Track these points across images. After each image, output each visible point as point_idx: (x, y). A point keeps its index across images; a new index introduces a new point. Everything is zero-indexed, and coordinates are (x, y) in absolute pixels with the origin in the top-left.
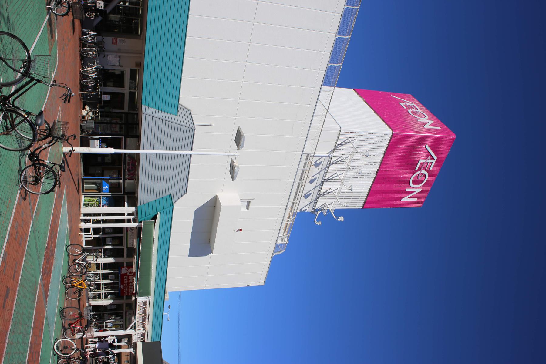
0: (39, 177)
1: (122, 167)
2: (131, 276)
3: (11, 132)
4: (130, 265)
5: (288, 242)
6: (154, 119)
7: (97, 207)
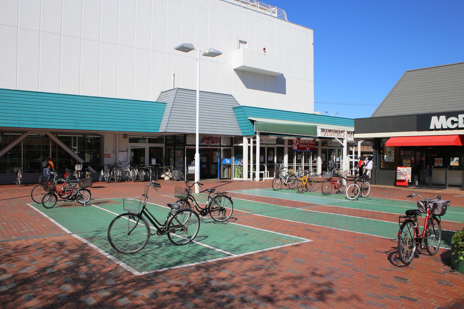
0: (219, 208)
1: (210, 148)
2: (299, 142)
3: (185, 227)
4: (291, 142)
5: (276, 7)
6: (170, 122)
7: (243, 168)
